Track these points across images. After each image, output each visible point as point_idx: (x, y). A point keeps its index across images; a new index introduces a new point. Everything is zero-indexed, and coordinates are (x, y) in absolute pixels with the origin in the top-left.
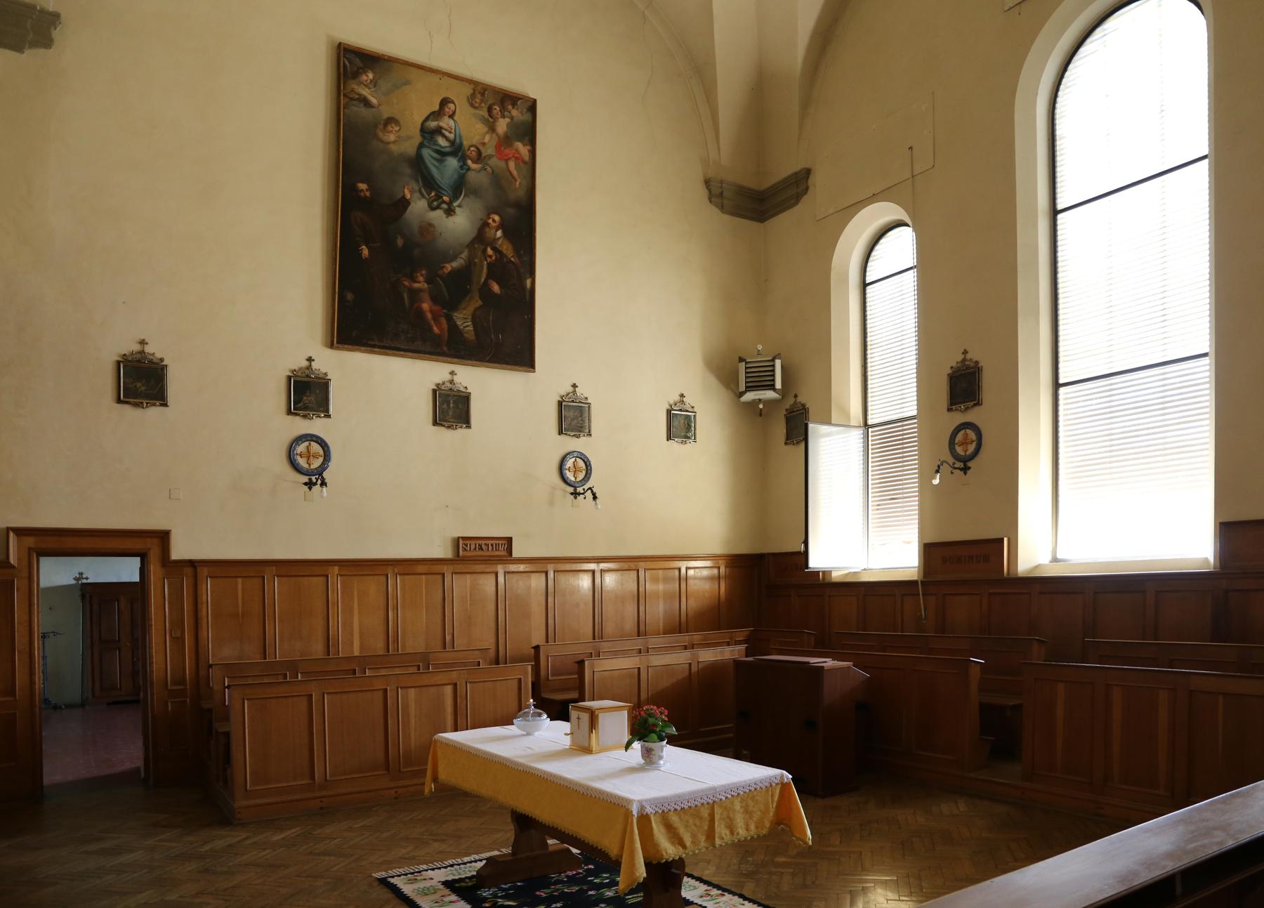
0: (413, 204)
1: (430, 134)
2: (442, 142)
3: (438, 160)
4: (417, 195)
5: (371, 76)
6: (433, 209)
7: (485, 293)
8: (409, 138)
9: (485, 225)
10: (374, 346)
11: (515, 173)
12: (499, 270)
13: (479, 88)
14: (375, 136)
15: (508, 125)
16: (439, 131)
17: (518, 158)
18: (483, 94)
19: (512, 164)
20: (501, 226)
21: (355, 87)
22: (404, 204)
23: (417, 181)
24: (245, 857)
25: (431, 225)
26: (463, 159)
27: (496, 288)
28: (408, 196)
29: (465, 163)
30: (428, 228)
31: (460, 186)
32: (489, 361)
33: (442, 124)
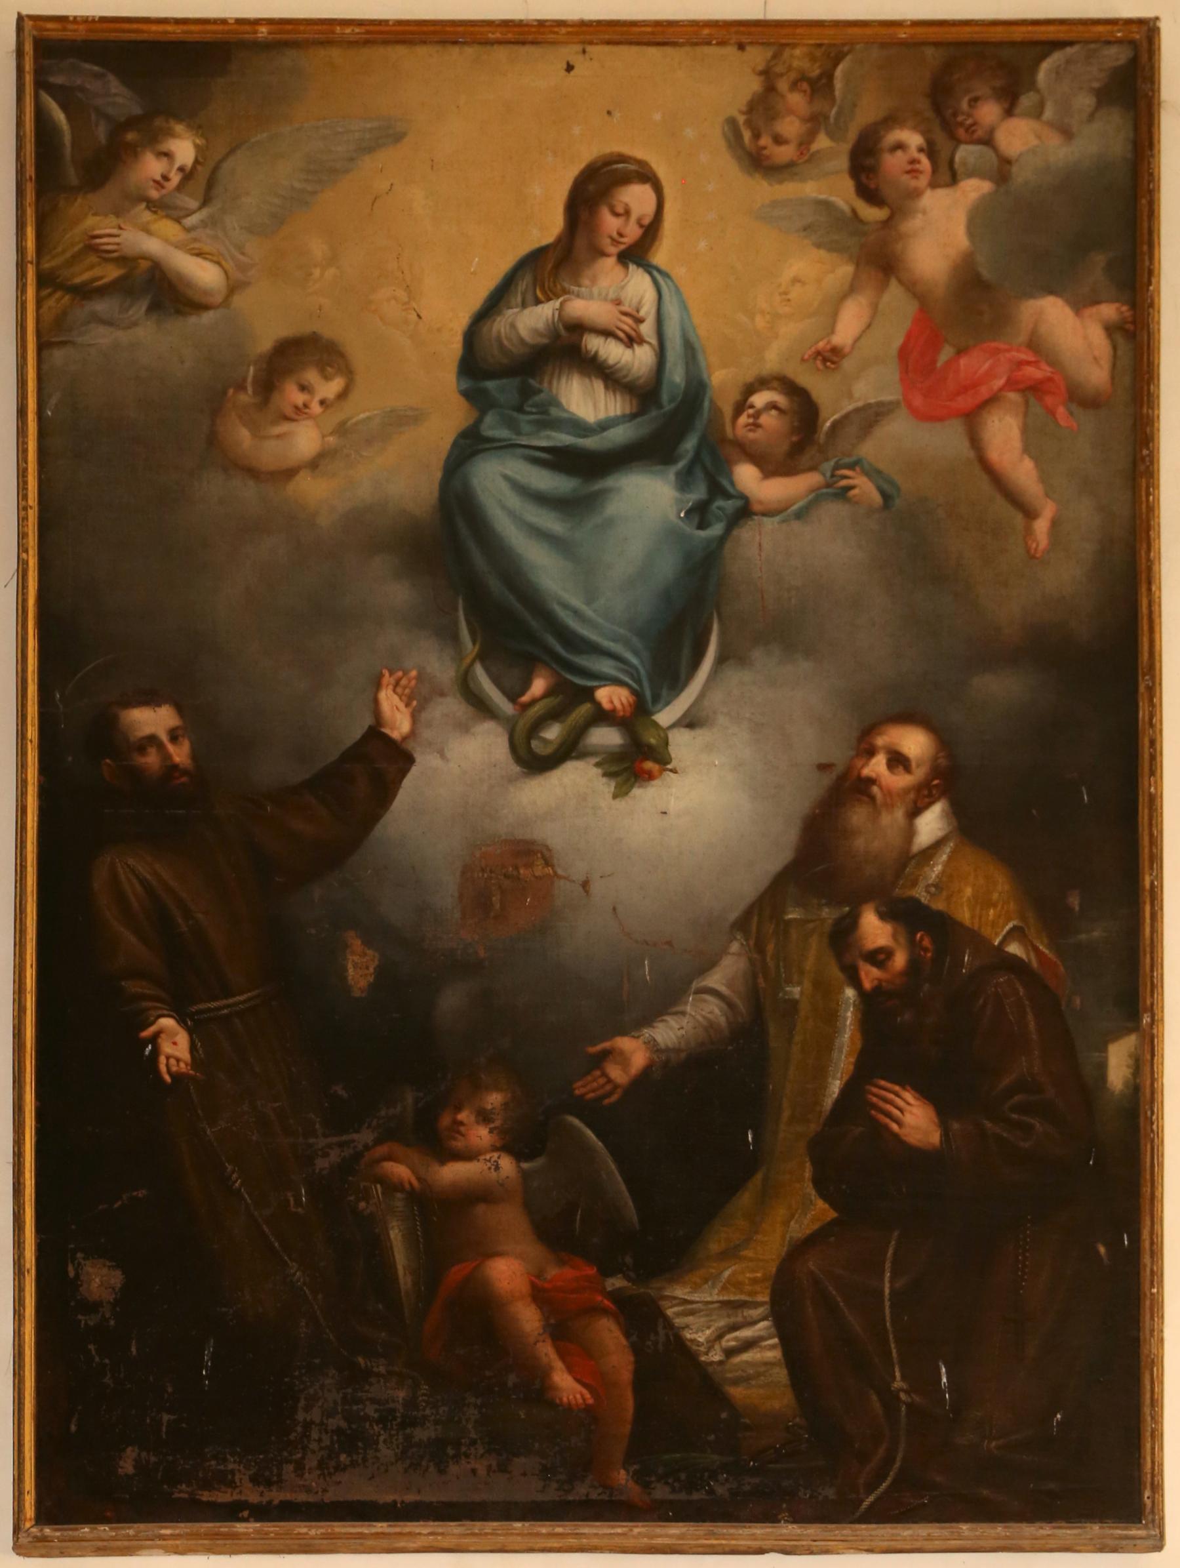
0: (425, 761)
1: (503, 376)
2: (583, 401)
4: (452, 706)
5: (184, 149)
6: (535, 763)
7: (853, 1157)
8: (401, 420)
9: (846, 789)
10: (232, 1512)
11: (1024, 473)
12: (937, 1019)
15: (980, 220)
16: (567, 349)
18: (820, 86)
19: (1004, 433)
21: (102, 225)
22: (380, 763)
24: (945, 857)
26: (709, 473)
27: (915, 1119)
28: (399, 723)
29: (717, 490)
30: (514, 872)
31: (689, 621)
32: (884, 1514)
33: (582, 307)
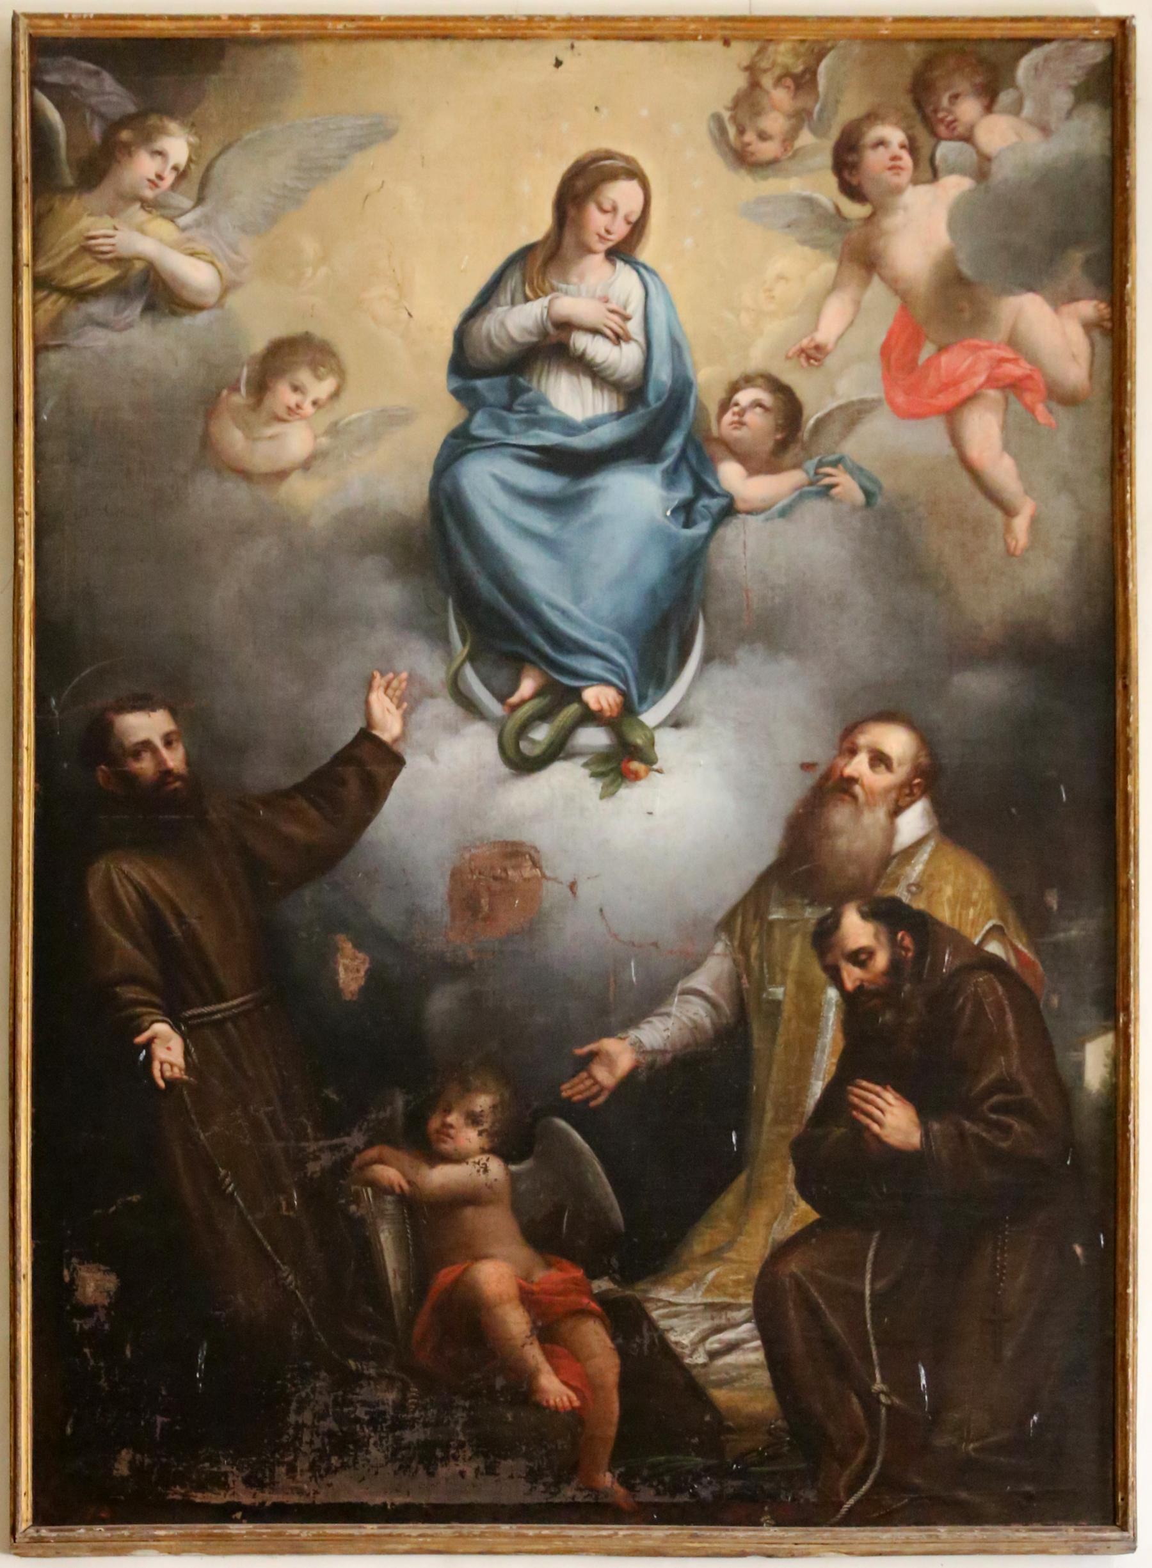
0: (415, 763)
1: (492, 374)
2: (571, 399)
3: (551, 504)
6: (524, 764)
7: (835, 1159)
8: (393, 419)
9: (830, 788)
10: (225, 1513)
12: (917, 1022)
13: (783, 54)
14: (209, 455)
15: (961, 218)
17: (1022, 385)
18: (804, 82)
19: (984, 430)
20: (928, 779)
22: (369, 766)
23: (439, 637)
25: (515, 852)
26: (695, 469)
27: (895, 1120)
28: (389, 726)
30: (499, 875)
31: (671, 624)
32: (859, 1518)
